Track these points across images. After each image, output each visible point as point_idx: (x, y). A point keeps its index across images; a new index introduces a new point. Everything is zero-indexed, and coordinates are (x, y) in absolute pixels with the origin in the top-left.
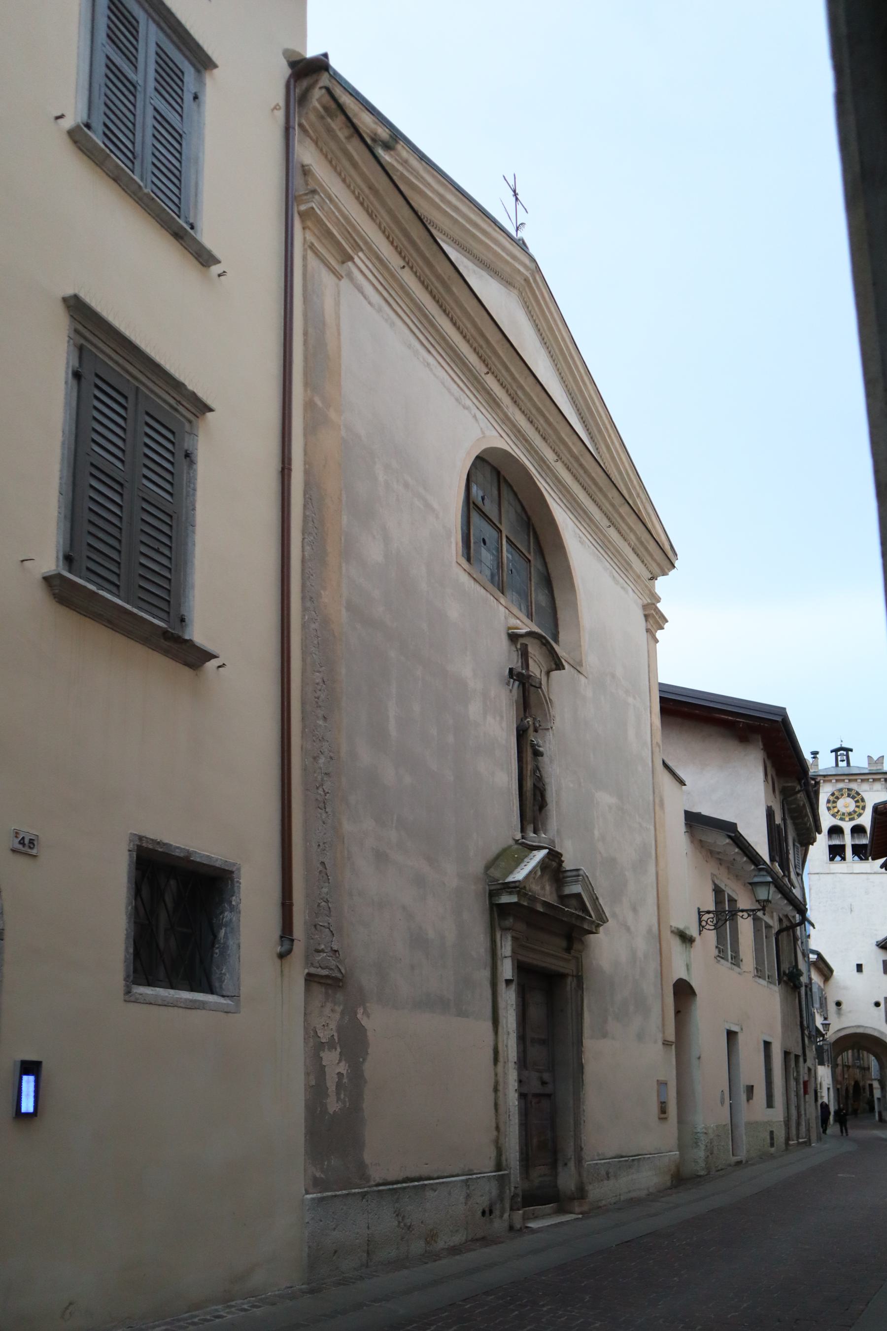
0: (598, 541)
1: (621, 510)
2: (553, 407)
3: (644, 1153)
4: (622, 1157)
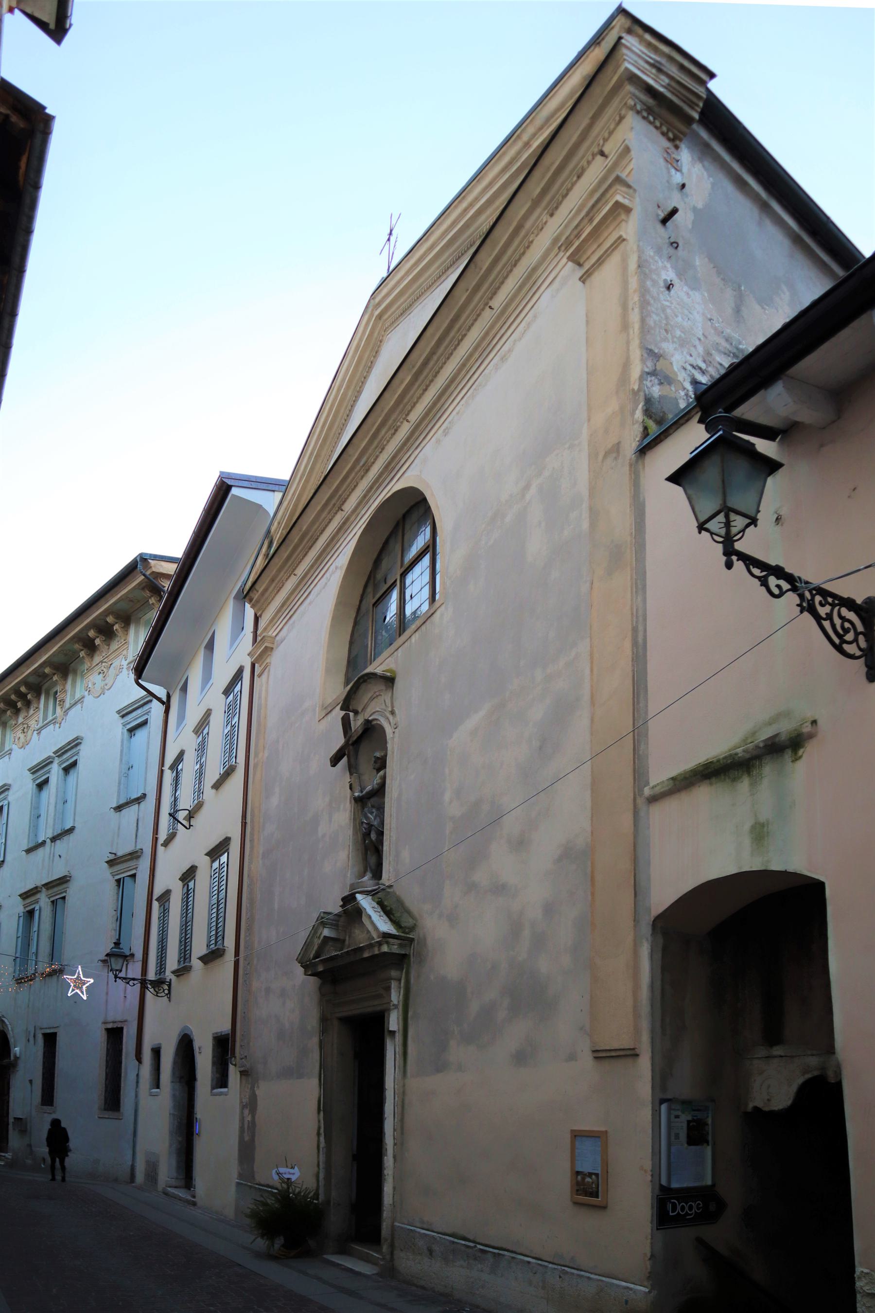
2: (377, 407)
3: (519, 1251)
4: (464, 1239)
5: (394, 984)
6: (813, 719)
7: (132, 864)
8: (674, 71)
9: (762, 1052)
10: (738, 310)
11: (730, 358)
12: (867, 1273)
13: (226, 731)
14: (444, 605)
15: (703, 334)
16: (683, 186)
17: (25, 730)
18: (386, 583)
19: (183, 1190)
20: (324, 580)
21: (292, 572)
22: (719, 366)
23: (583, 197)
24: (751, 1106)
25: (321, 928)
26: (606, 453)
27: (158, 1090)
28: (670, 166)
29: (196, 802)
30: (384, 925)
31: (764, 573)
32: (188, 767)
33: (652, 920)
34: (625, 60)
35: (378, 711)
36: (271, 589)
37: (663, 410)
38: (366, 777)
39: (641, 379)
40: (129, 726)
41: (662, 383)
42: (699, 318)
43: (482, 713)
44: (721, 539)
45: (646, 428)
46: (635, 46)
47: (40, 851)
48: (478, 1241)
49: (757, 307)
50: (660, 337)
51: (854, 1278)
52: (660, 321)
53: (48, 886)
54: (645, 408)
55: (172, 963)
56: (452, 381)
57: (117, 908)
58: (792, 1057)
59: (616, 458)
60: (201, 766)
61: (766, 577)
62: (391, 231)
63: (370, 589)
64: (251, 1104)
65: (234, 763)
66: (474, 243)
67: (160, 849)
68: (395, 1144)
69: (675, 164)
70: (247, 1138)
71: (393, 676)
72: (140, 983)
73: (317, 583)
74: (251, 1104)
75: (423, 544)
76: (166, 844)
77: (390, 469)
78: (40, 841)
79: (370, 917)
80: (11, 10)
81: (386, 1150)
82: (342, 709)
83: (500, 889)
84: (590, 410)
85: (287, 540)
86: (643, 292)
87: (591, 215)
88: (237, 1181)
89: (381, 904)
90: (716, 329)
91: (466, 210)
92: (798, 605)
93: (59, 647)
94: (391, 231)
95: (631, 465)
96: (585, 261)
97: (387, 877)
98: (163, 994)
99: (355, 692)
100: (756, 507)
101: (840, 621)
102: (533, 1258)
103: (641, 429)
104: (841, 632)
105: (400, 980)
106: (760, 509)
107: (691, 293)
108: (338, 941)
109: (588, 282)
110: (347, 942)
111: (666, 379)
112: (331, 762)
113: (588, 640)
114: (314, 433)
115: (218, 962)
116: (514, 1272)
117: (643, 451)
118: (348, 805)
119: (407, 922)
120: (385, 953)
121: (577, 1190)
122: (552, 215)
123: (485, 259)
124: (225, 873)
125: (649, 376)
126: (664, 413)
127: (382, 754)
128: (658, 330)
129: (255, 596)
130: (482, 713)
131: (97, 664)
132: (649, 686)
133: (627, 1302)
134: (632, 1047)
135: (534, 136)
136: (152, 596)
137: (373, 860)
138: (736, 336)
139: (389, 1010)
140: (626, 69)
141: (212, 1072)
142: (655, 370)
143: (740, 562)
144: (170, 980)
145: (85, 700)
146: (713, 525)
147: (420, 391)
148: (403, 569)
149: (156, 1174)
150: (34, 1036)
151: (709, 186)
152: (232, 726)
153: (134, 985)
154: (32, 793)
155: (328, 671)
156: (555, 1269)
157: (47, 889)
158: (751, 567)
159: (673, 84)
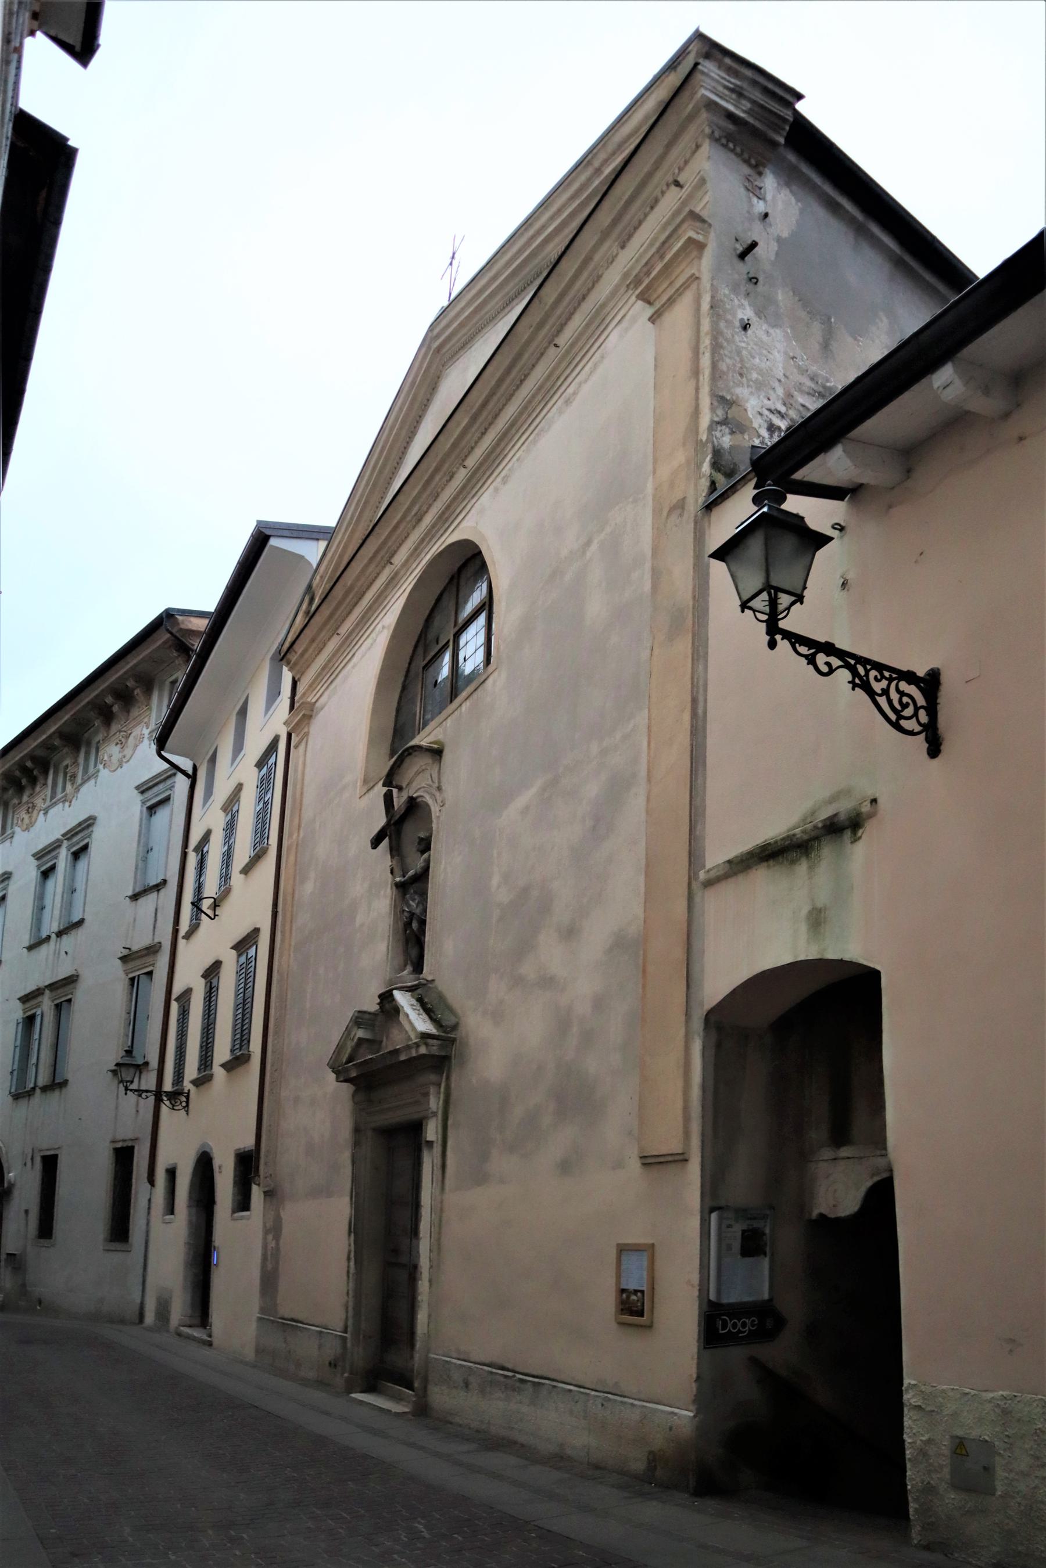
0: (349, 650)
1: (551, 300)
4: (503, 1368)
5: (432, 1090)
6: (872, 798)
7: (149, 959)
8: (757, 96)
9: (827, 1153)
10: (826, 346)
11: (814, 398)
12: (915, 1385)
13: (258, 809)
14: (497, 670)
15: (784, 375)
16: (766, 215)
17: (30, 810)
18: (437, 643)
19: (201, 1329)
20: (369, 641)
21: (335, 632)
22: (801, 409)
23: (655, 231)
24: (815, 1214)
25: (355, 1028)
26: (671, 508)
27: (172, 1216)
28: (751, 194)
29: (223, 888)
30: (422, 1024)
31: (812, 651)
32: (215, 851)
33: (705, 1014)
34: (702, 86)
35: (424, 787)
36: (311, 651)
37: (734, 461)
38: (409, 860)
39: (711, 429)
40: (149, 804)
41: (734, 432)
42: (778, 357)
43: (533, 790)
44: (764, 618)
45: (713, 484)
46: (713, 72)
47: (44, 949)
48: (518, 1369)
49: (850, 340)
50: (734, 382)
51: (902, 1391)
52: (734, 365)
53: (53, 987)
54: (713, 460)
55: (191, 1071)
56: (512, 425)
57: (131, 1010)
58: (861, 1158)
59: (681, 515)
60: (229, 848)
61: (814, 655)
62: (454, 254)
63: (420, 650)
64: (274, 1229)
65: (265, 845)
66: (541, 273)
67: (181, 943)
68: (431, 1267)
69: (757, 192)
70: (270, 1266)
71: (441, 748)
72: (154, 1095)
73: (362, 644)
74: (274, 1229)
75: (479, 601)
76: (188, 936)
77: (446, 518)
78: (44, 936)
79: (407, 1016)
80: (32, 33)
81: (421, 1273)
82: (384, 785)
83: (547, 982)
84: (655, 461)
85: (329, 597)
86: (716, 335)
87: (662, 252)
88: (259, 1315)
89: (420, 1000)
90: (799, 367)
91: (533, 238)
92: (849, 682)
93: (72, 716)
94: (454, 254)
95: (696, 523)
96: (655, 300)
97: (427, 973)
98: (180, 1107)
99: (399, 766)
100: (802, 584)
101: (899, 696)
102: (576, 1386)
103: (708, 484)
104: (899, 707)
105: (439, 1085)
106: (808, 585)
107: (771, 331)
108: (373, 1043)
109: (658, 322)
110: (384, 1044)
111: (737, 427)
112: (372, 843)
113: (646, 711)
114: (355, 495)
115: (241, 1070)
116: (554, 1402)
117: (709, 507)
118: (389, 890)
119: (449, 1020)
120: (424, 1055)
121: (622, 1310)
122: (623, 247)
123: (550, 294)
124: (252, 969)
125: (718, 425)
126: (735, 464)
127: (428, 834)
128: (730, 375)
129: (293, 657)
130: (533, 790)
131: (115, 734)
132: (707, 761)
133: (671, 1429)
134: (680, 1152)
135: (606, 162)
136: (179, 656)
137: (414, 952)
138: (823, 373)
139: (426, 1118)
140: (703, 95)
141: (233, 1194)
142: (727, 418)
143: (786, 642)
144: (189, 1091)
145: (100, 774)
146: (756, 603)
147: (478, 435)
148: (457, 629)
149: (169, 1312)
150: (32, 1159)
151: (798, 212)
152: (264, 803)
153: (147, 1097)
154: (36, 882)
155: (371, 742)
156: (597, 1396)
157: (51, 991)
158: (797, 645)
159: (756, 109)
